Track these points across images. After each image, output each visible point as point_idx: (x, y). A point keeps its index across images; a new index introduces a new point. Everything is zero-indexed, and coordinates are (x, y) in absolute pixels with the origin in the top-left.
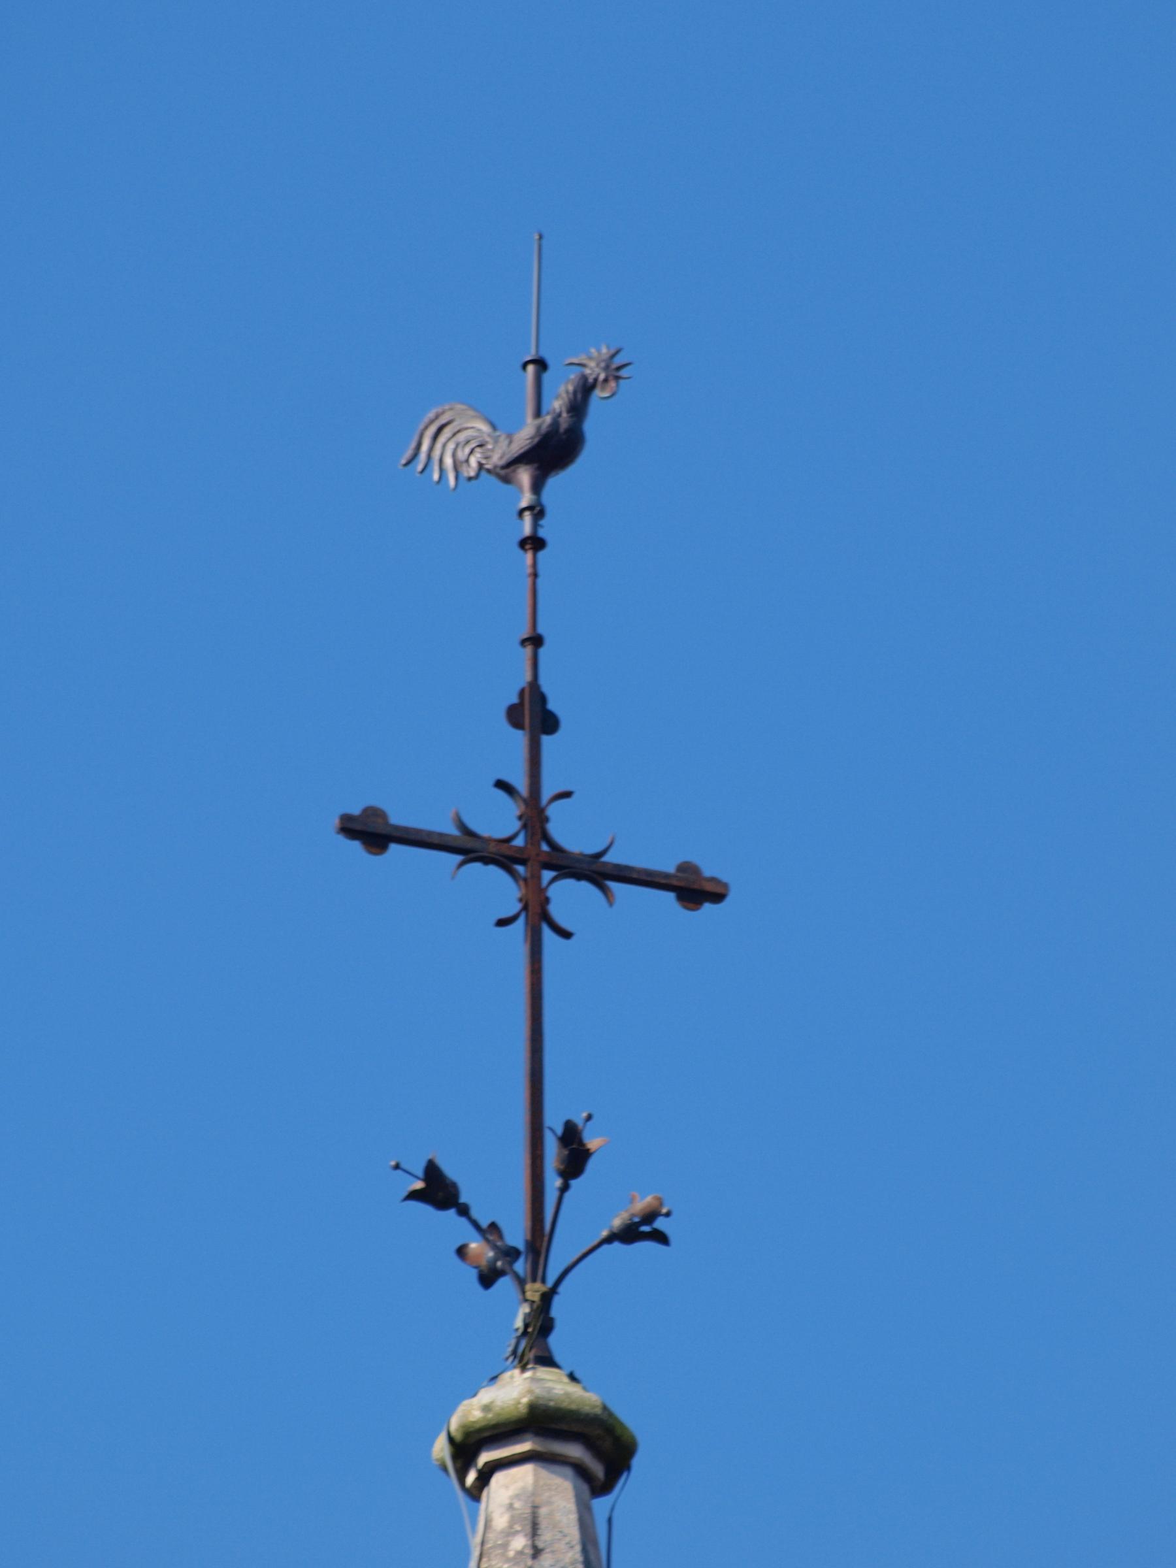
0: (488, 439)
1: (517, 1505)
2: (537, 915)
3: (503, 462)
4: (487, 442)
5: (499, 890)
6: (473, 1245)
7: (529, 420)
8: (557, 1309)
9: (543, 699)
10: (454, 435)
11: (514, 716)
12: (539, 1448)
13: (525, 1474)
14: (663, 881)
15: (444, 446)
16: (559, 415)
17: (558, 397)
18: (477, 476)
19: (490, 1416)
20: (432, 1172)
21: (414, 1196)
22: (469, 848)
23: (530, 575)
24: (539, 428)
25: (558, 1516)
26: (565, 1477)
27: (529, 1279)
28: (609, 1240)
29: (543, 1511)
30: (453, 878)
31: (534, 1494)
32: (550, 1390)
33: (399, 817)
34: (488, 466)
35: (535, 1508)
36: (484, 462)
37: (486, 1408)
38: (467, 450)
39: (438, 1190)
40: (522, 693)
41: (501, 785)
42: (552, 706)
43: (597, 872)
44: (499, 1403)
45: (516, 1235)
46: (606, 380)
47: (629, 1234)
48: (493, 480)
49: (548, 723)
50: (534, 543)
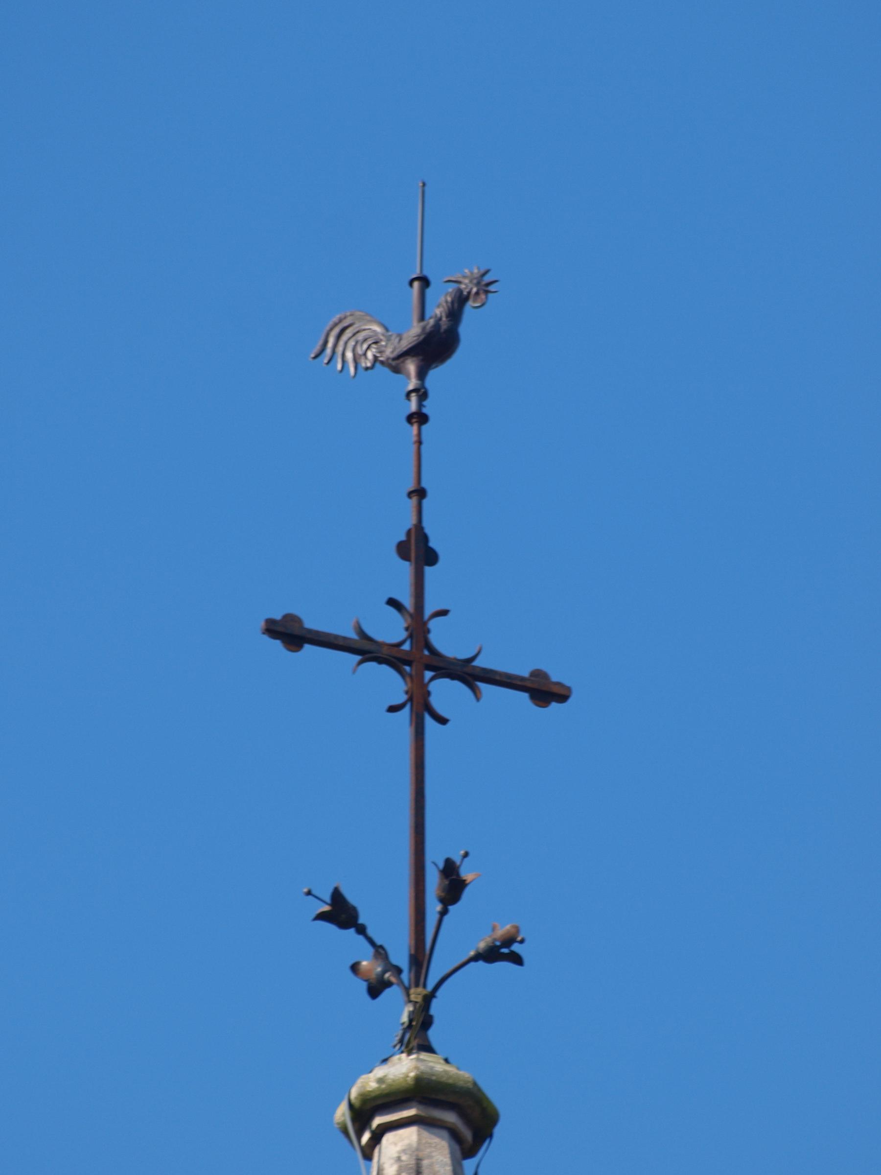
0: (382, 337)
1: (404, 1158)
2: (420, 707)
3: (392, 356)
4: (381, 340)
5: (390, 684)
6: (364, 963)
7: (415, 323)
8: (435, 1008)
9: (425, 538)
10: (354, 335)
11: (403, 550)
12: (423, 1114)
13: (410, 1135)
14: (519, 683)
15: (346, 343)
16: (440, 319)
17: (438, 306)
18: (373, 367)
19: (383, 1086)
20: (337, 897)
21: (322, 917)
22: (366, 649)
23: (415, 442)
24: (424, 328)
25: (437, 1168)
26: (442, 1138)
27: (413, 985)
28: (476, 958)
29: (425, 1163)
30: (354, 671)
31: (418, 1149)
32: (432, 1068)
33: (312, 623)
34: (381, 359)
35: (419, 1161)
36: (378, 355)
37: (380, 1081)
38: (365, 346)
39: (341, 913)
40: (409, 533)
41: (393, 603)
42: (432, 544)
43: (469, 674)
44: (391, 1077)
45: (400, 956)
46: (477, 293)
47: (491, 955)
48: (386, 371)
49: (430, 557)
50: (419, 418)
